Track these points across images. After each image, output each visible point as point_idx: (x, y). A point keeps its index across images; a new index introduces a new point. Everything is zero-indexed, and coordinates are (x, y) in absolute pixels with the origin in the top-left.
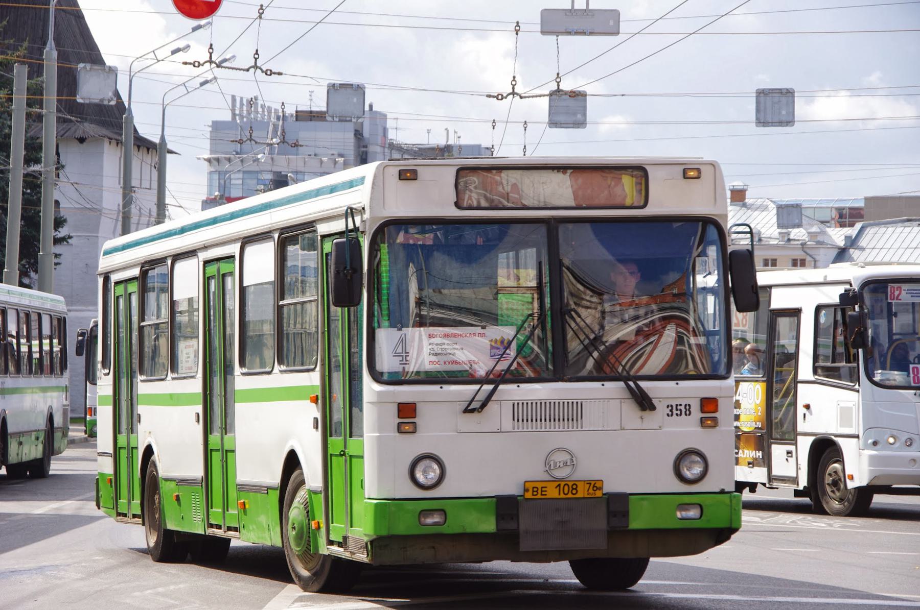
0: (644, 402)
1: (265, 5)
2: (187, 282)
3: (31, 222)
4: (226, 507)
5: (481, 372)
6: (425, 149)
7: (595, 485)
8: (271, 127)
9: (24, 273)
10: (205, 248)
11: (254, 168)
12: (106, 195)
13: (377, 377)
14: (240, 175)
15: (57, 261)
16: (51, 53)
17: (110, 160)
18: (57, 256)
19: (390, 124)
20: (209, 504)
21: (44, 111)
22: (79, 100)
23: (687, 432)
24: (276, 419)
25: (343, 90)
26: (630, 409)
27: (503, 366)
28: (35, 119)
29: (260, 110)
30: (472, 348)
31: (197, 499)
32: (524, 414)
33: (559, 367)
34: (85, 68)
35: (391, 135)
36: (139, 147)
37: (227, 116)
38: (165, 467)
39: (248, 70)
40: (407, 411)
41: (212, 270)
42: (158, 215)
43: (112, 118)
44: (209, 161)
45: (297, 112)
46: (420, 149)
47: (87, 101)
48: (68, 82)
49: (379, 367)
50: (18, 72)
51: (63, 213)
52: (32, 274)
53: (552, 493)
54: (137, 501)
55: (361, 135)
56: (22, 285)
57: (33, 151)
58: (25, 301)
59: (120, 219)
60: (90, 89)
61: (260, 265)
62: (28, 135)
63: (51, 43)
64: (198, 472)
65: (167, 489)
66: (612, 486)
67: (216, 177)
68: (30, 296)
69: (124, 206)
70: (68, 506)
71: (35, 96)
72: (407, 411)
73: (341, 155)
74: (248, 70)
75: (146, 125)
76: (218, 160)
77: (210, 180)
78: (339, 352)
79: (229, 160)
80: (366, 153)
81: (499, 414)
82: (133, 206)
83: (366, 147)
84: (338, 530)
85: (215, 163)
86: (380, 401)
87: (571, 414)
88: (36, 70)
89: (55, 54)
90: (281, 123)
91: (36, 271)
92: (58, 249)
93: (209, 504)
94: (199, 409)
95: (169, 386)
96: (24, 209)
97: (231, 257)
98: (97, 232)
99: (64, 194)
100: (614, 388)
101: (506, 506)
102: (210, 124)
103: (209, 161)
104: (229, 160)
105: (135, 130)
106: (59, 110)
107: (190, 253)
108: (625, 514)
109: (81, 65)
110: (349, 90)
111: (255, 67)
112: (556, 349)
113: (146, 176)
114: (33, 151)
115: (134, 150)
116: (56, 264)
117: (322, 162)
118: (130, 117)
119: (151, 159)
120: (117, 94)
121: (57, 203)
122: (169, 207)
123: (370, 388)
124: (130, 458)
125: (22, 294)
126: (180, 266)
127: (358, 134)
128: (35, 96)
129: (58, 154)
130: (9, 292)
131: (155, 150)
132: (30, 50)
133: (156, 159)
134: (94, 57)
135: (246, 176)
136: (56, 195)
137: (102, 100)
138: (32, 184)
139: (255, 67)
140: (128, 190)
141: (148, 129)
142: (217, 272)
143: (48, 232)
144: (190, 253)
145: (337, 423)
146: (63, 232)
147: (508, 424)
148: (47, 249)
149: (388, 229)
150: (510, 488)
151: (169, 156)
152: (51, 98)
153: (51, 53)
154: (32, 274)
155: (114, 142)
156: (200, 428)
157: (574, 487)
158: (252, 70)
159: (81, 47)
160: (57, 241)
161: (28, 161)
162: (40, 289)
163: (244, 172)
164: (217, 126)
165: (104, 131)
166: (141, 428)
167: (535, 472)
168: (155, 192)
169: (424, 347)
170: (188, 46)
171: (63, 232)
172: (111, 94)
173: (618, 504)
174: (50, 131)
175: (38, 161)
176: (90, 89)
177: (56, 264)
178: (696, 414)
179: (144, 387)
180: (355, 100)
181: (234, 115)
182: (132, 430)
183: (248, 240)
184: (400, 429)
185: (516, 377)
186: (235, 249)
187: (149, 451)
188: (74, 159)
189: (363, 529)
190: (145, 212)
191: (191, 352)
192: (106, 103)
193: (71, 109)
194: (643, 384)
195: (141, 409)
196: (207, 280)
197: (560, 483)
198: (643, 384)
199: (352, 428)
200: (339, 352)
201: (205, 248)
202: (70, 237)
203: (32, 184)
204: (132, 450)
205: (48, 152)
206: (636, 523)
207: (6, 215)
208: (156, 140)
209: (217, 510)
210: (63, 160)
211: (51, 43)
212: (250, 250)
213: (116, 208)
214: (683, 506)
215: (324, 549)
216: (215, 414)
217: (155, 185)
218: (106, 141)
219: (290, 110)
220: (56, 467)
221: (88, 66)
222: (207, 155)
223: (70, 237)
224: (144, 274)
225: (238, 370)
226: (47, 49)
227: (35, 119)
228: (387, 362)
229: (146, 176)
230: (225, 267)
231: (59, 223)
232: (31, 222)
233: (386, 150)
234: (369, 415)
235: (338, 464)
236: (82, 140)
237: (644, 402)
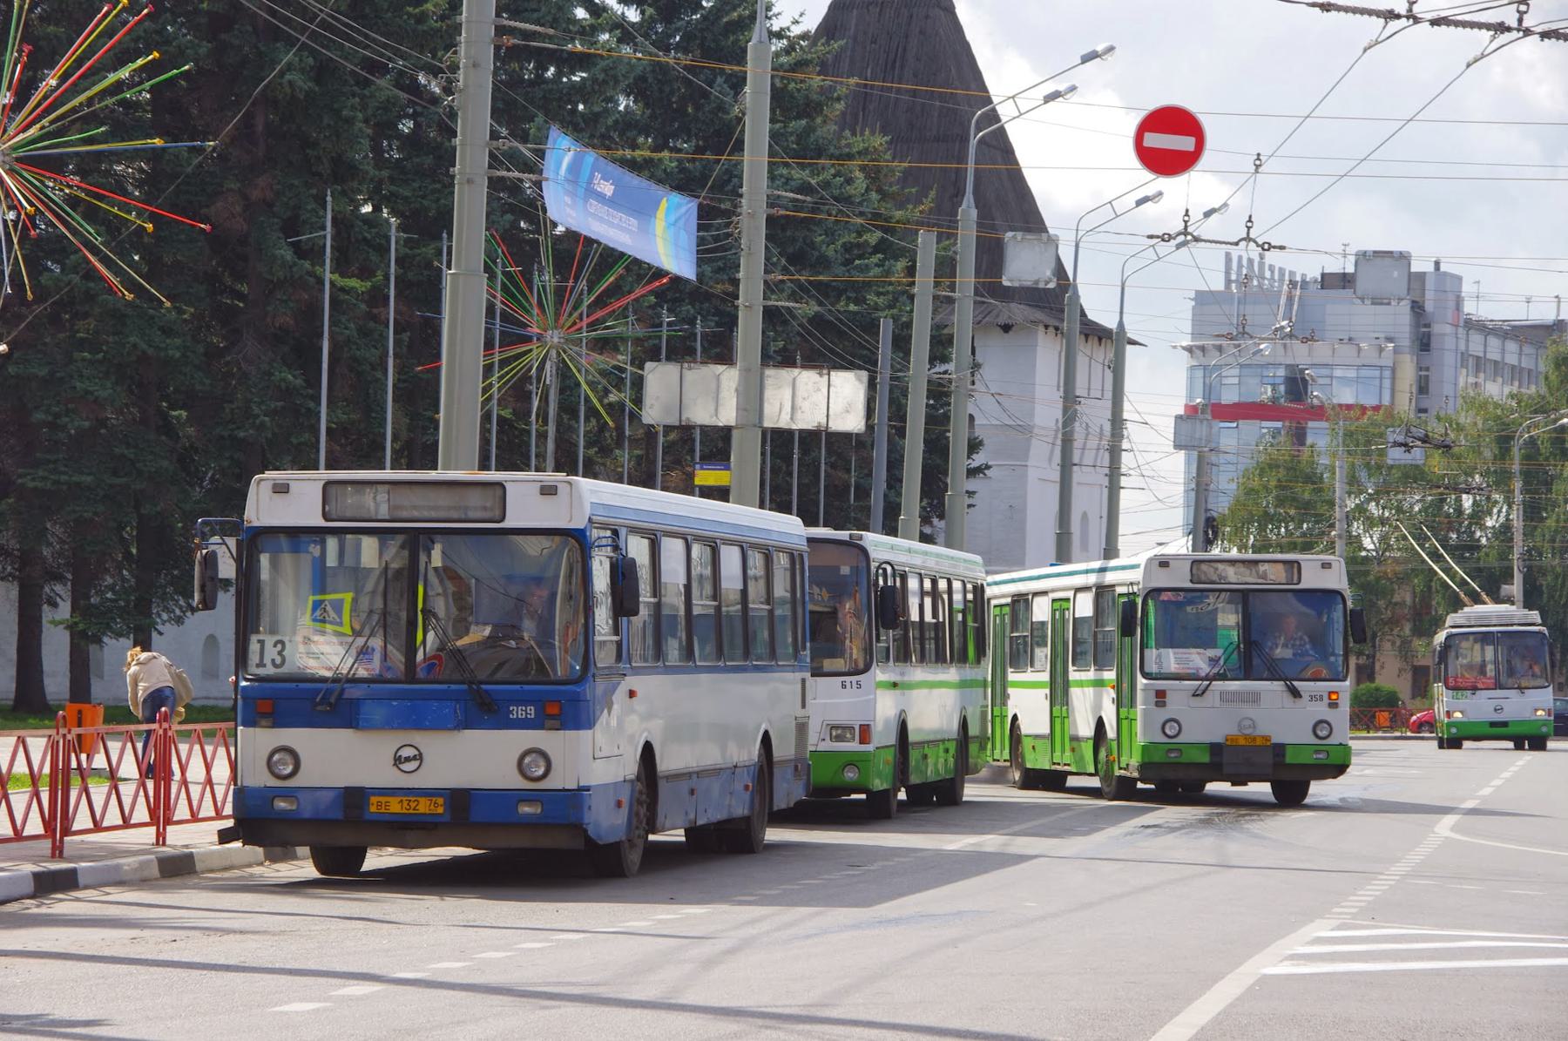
0: (1296, 693)
1: (1265, 153)
2: (1041, 611)
3: (937, 448)
4: (1063, 751)
5: (1203, 674)
6: (1522, 327)
7: (1267, 738)
8: (1283, 301)
9: (925, 520)
10: (1053, 591)
11: (1258, 360)
12: (1038, 409)
13: (1146, 675)
14: (1236, 371)
15: (971, 501)
16: (968, 211)
17: (1047, 354)
18: (970, 494)
19: (1467, 288)
20: (1053, 751)
21: (956, 295)
22: (1006, 283)
23: (1321, 710)
24: (1092, 700)
25: (1378, 261)
26: (1287, 697)
27: (1215, 670)
28: (943, 303)
29: (1268, 274)
30: (1198, 660)
31: (1043, 746)
32: (1226, 697)
33: (1247, 673)
34: (1014, 237)
35: (1469, 307)
36: (1087, 336)
37: (1218, 284)
38: (1026, 728)
39: (1237, 244)
40: (1161, 694)
41: (1057, 605)
42: (1113, 435)
43: (1053, 302)
44: (1189, 349)
45: (1323, 275)
46: (1515, 327)
47: (1016, 284)
48: (991, 256)
49: (1147, 670)
50: (924, 242)
51: (978, 432)
52: (935, 521)
53: (1242, 742)
54: (1007, 751)
55: (1422, 308)
56: (926, 538)
57: (941, 346)
58: (931, 563)
59: (1059, 442)
60: (1023, 265)
61: (1084, 607)
62: (938, 318)
63: (969, 199)
64: (1046, 730)
65: (1027, 744)
66: (1275, 740)
67: (1200, 373)
68: (938, 555)
69: (1065, 425)
70: (990, 842)
71: (946, 267)
72: (1161, 694)
73: (1390, 340)
74: (1237, 244)
75: (1098, 306)
76: (1203, 349)
77: (1191, 379)
78: (1127, 660)
79: (1220, 348)
80: (1429, 335)
81: (1212, 697)
82: (1077, 424)
83: (1428, 325)
84: (1124, 760)
85: (1199, 353)
86: (1145, 689)
87: (1255, 698)
88: (947, 233)
89: (974, 213)
90: (1298, 292)
91: (941, 517)
92: (972, 485)
93: (1053, 751)
94: (1047, 691)
95: (1028, 676)
96: (926, 431)
97: (1067, 600)
98: (1026, 457)
99: (982, 408)
100: (1278, 686)
101: (1215, 749)
102: (1193, 295)
103: (1189, 349)
104: (1220, 348)
105: (1083, 314)
106: (976, 294)
107: (1044, 593)
108: (1284, 756)
109: (1010, 234)
110: (1388, 261)
111: (1248, 239)
112: (1251, 660)
113: (1096, 385)
114: (941, 346)
115: (1079, 340)
116: (970, 506)
117: (1359, 350)
118: (1076, 295)
119: (1103, 354)
120: (1060, 270)
121: (971, 418)
122: (1129, 425)
123: (1141, 681)
124: (1002, 723)
125: (926, 553)
126: (1037, 600)
127: (1417, 308)
128: (946, 267)
129: (973, 353)
130: (910, 550)
131: (1110, 341)
132: (938, 209)
133: (1111, 355)
134: (1028, 217)
135: (1246, 371)
136: (971, 409)
137: (1037, 282)
138: (939, 392)
139: (1248, 239)
140: (1070, 400)
141: (1101, 312)
142: (1060, 606)
143: (959, 460)
144: (1044, 593)
145: (1124, 700)
146: (979, 459)
147: (1217, 703)
148: (957, 481)
149: (1153, 593)
150: (1218, 739)
151: (1129, 347)
152: (967, 278)
153: (968, 211)
154: (935, 521)
155: (1051, 330)
156: (1047, 703)
157: (1254, 739)
158: (1243, 244)
159: (1011, 205)
160: (973, 472)
161: (933, 360)
162: (948, 545)
163: (1242, 366)
164: (1203, 299)
165: (1039, 315)
166: (1010, 703)
167: (1234, 731)
168: (1109, 404)
169: (1171, 660)
170: (1160, 194)
171: (979, 459)
172: (1048, 273)
173: (1280, 749)
174: (963, 318)
175: (945, 359)
176: (1023, 265)
177: (970, 506)
178: (1326, 701)
179: (1012, 676)
180: (1396, 274)
181: (1228, 282)
182: (1004, 704)
183: (1078, 590)
184: (1157, 704)
185: (1222, 677)
186: (1070, 594)
187: (1015, 718)
188: (996, 357)
189: (1135, 761)
190: (1095, 429)
191: (1043, 654)
192: (1041, 285)
193: (991, 286)
194: (1296, 683)
195: (1010, 691)
196: (1054, 611)
197: (1246, 737)
198: (1296, 683)
199: (1133, 704)
200: (1127, 660)
201: (1053, 591)
202: (988, 467)
203: (939, 392)
204: (1003, 717)
205: (959, 350)
206: (1289, 759)
207: (904, 437)
208: (1110, 322)
209: (1057, 754)
210: (979, 358)
211: (969, 199)
212: (1079, 596)
213: (1052, 425)
214: (1317, 752)
215: (1118, 773)
216: (1059, 692)
217: (1109, 395)
218: (1041, 328)
219: (1314, 273)
220: (972, 792)
221: (1019, 235)
222: (1187, 342)
223: (988, 467)
224: (1014, 602)
225: (1071, 668)
226: (964, 206)
227: (943, 303)
228: (1152, 667)
229: (1096, 385)
230: (1065, 605)
231: (974, 446)
232: (937, 448)
233: (1461, 330)
234: (1139, 696)
235: (1125, 723)
236: (1006, 328)
237: (1296, 693)
